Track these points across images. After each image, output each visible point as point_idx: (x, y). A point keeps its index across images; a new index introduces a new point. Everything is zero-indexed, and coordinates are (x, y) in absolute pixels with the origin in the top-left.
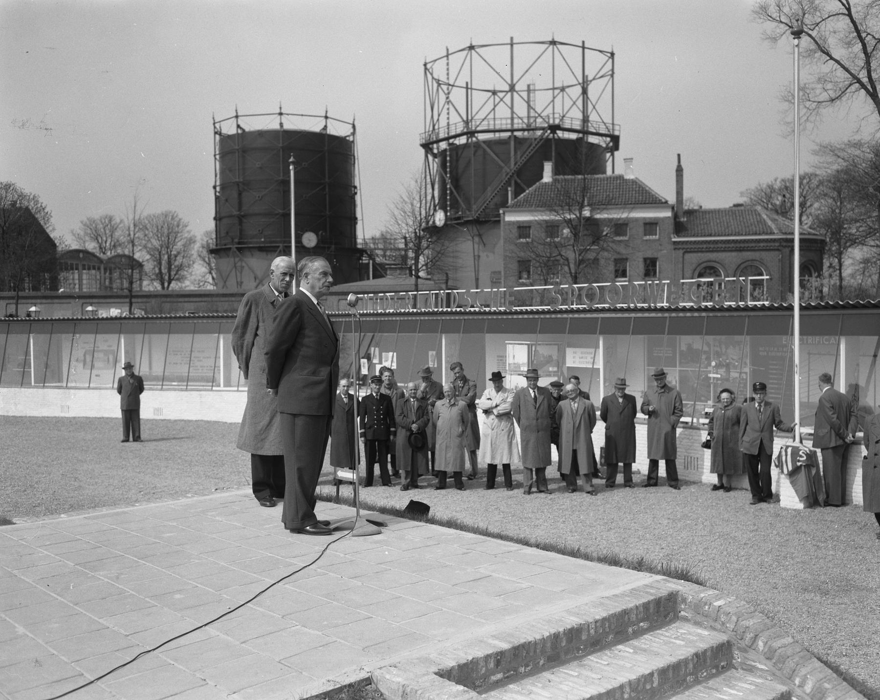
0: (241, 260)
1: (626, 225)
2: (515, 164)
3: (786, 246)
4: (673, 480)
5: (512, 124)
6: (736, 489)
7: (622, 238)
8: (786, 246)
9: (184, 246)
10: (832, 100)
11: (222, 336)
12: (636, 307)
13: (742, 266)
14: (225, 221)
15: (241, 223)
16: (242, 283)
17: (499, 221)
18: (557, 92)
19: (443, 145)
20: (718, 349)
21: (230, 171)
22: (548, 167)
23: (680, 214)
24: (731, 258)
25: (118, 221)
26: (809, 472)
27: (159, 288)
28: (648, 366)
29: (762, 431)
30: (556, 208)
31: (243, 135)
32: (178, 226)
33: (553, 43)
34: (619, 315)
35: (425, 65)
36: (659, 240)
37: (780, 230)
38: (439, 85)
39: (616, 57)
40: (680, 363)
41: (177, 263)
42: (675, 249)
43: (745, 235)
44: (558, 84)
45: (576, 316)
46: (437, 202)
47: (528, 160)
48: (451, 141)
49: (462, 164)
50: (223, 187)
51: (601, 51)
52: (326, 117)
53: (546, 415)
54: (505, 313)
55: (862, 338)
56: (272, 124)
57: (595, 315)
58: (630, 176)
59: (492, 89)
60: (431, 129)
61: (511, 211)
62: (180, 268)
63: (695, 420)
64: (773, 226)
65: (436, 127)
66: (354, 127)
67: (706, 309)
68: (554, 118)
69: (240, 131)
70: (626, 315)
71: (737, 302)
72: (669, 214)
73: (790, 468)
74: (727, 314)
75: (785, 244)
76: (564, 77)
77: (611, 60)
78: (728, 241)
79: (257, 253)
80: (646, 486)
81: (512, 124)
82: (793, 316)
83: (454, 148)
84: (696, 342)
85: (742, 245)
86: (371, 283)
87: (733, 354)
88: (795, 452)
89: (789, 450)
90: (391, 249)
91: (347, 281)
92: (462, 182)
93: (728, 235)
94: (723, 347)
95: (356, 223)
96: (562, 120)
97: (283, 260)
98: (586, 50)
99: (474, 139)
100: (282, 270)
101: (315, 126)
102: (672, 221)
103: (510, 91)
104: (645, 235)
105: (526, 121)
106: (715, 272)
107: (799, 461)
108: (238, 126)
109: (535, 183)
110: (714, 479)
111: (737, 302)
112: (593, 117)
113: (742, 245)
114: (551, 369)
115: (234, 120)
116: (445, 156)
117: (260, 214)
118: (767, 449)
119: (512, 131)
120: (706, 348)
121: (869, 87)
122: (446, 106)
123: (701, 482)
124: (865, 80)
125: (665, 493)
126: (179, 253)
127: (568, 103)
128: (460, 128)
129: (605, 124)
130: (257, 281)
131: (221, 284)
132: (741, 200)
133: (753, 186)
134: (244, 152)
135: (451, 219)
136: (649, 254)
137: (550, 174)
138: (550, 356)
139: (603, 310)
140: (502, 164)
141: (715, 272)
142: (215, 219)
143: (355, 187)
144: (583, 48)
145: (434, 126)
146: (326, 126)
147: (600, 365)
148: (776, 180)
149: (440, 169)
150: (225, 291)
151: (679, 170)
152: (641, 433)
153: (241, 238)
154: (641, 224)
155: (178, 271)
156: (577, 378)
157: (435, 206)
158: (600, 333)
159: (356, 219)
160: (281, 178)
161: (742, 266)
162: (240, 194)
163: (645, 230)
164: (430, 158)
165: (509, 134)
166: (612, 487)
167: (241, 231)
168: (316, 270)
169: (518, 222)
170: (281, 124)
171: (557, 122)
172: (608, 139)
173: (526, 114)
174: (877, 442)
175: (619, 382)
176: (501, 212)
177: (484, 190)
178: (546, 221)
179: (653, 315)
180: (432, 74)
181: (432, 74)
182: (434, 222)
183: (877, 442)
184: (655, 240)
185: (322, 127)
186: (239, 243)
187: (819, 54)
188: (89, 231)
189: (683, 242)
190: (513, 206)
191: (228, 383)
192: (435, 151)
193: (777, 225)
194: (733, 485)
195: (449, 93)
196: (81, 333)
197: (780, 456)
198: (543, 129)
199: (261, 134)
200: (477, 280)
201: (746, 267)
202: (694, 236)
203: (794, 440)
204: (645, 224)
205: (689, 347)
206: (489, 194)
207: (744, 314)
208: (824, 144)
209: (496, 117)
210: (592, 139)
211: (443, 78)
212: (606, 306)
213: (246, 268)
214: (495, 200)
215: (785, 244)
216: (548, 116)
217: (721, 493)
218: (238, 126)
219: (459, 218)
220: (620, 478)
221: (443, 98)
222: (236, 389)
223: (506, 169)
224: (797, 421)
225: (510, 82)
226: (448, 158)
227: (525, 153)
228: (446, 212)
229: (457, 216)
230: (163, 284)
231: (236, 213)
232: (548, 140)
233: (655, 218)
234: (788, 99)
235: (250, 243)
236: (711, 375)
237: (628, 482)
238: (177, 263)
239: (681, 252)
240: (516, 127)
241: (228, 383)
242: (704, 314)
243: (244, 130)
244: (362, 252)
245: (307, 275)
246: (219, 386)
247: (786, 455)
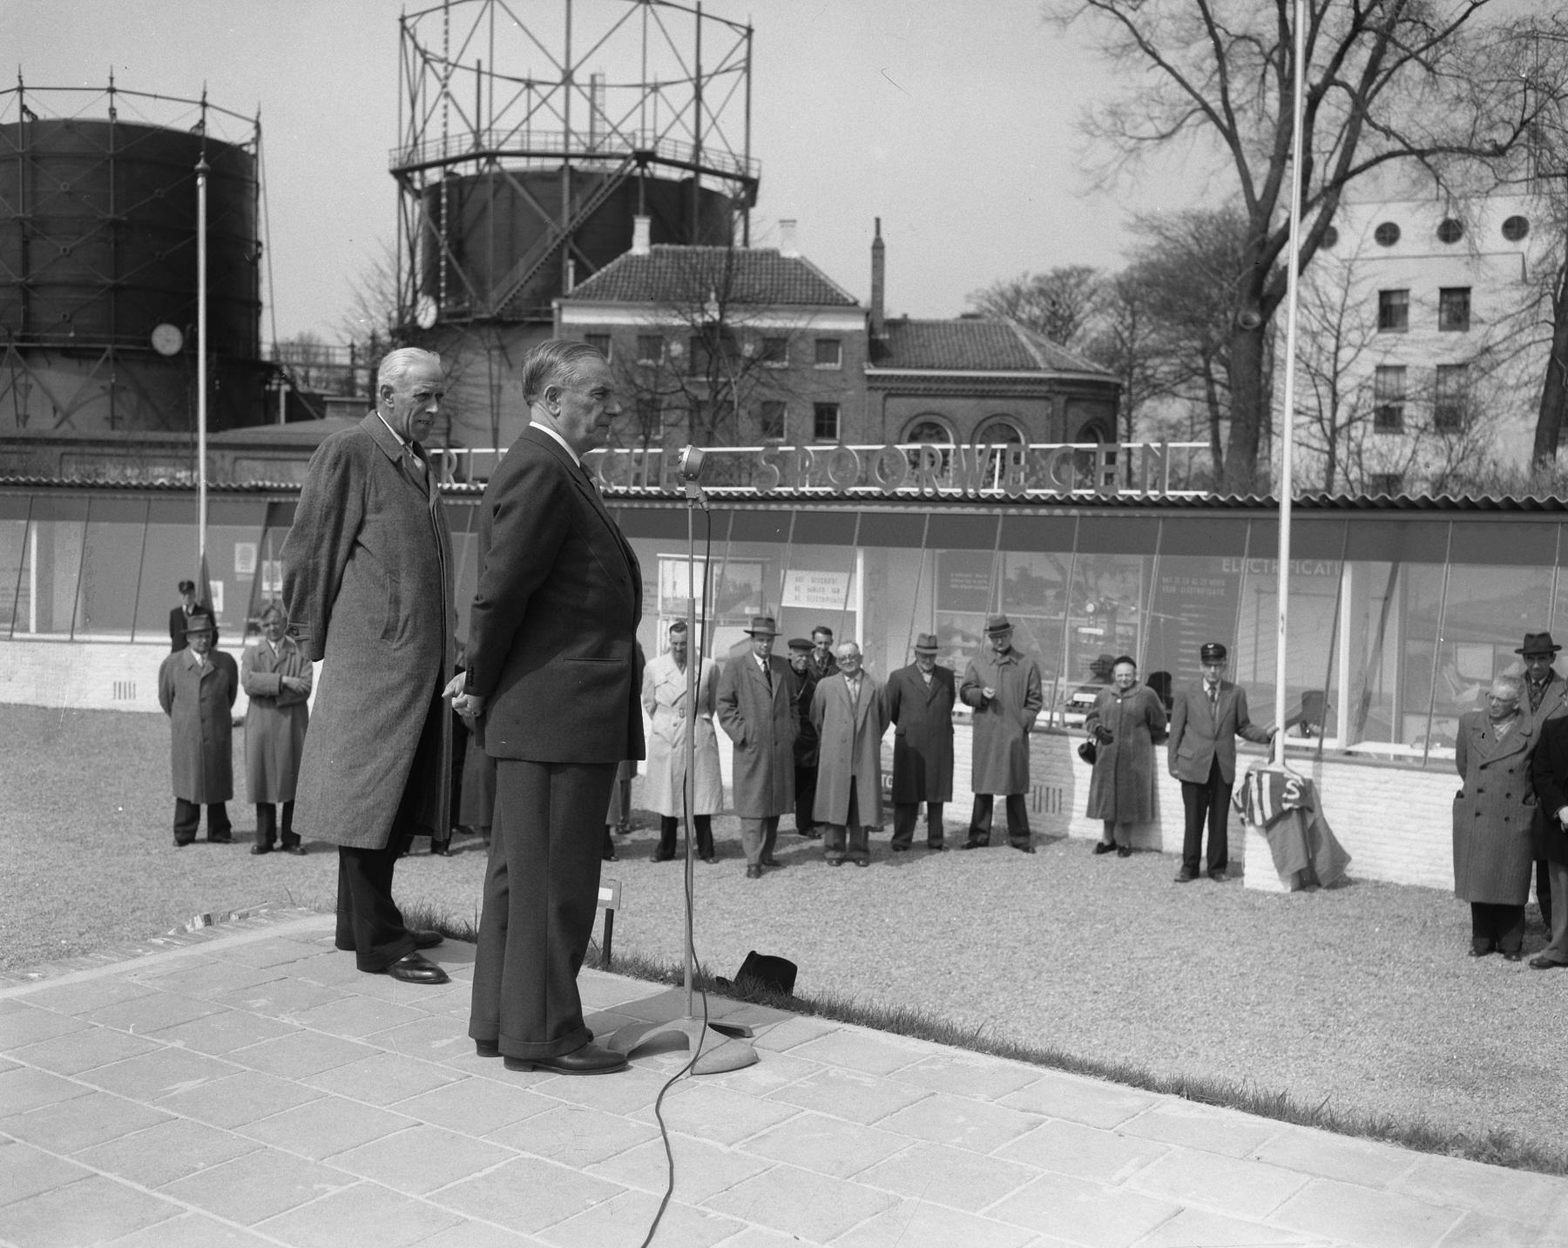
0: (25, 372)
2: (571, 219)
3: (1059, 393)
4: (1020, 834)
5: (567, 144)
6: (1139, 850)
8: (1059, 393)
10: (1163, 137)
11: (34, 526)
12: (936, 494)
13: (985, 425)
15: (27, 300)
16: (27, 417)
17: (550, 324)
18: (648, 90)
19: (434, 175)
20: (1081, 579)
22: (642, 227)
23: (878, 326)
24: (966, 410)
26: (1303, 822)
28: (941, 607)
29: (1216, 738)
30: (679, 304)
34: (900, 509)
35: (402, 20)
36: (841, 371)
37: (1050, 363)
38: (426, 61)
39: (755, 36)
40: (1004, 603)
42: (870, 389)
43: (992, 369)
44: (650, 80)
45: (810, 507)
46: (419, 281)
47: (595, 214)
48: (449, 167)
49: (471, 210)
51: (729, 24)
52: (204, 105)
53: (786, 702)
54: (659, 497)
55: (1374, 564)
57: (848, 508)
58: (790, 253)
59: (524, 76)
60: (411, 142)
61: (572, 305)
63: (1056, 717)
64: (1038, 357)
65: (420, 141)
66: (258, 126)
67: (1081, 502)
68: (644, 140)
69: (26, 119)
70: (914, 509)
71: (1144, 491)
72: (859, 324)
73: (1269, 815)
74: (1121, 513)
75: (1057, 388)
76: (664, 67)
77: (745, 42)
78: (963, 380)
80: (969, 847)
81: (567, 144)
82: (1277, 520)
83: (456, 183)
84: (1040, 565)
85: (986, 387)
86: (282, 430)
87: (1109, 587)
88: (1278, 782)
89: (1266, 779)
90: (319, 367)
91: (239, 423)
92: (470, 246)
93: (962, 368)
94: (1091, 575)
95: (259, 313)
96: (657, 140)
97: (412, 360)
98: (703, 19)
100: (416, 387)
102: (866, 338)
103: (562, 83)
104: (818, 361)
105: (587, 140)
106: (938, 433)
107: (1286, 801)
108: (24, 108)
109: (617, 256)
110: (1096, 830)
111: (1144, 491)
112: (711, 142)
113: (986, 387)
114: (747, 611)
115: (16, 95)
116: (439, 196)
118: (1224, 772)
119: (567, 156)
120: (1056, 577)
121: (1225, 122)
122: (442, 101)
123: (1066, 836)
124: (1216, 105)
125: (999, 861)
127: (665, 117)
128: (467, 145)
129: (734, 156)
130: (59, 415)
132: (971, 308)
133: (987, 284)
134: (34, 159)
135: (449, 316)
136: (825, 398)
138: (747, 586)
139: (868, 498)
140: (547, 219)
141: (938, 433)
143: (259, 244)
144: (699, 14)
145: (416, 139)
146: (202, 122)
147: (857, 605)
148: (1025, 276)
149: (427, 219)
151: (878, 248)
152: (963, 740)
153: (26, 329)
154: (812, 340)
156: (828, 632)
157: (415, 293)
158: (859, 544)
159: (259, 304)
160: (111, 216)
161: (985, 425)
162: (26, 243)
163: (817, 354)
164: (408, 198)
165: (559, 162)
166: (905, 849)
167: (27, 315)
168: (583, 382)
169: (587, 326)
170: (112, 111)
171: (649, 146)
172: (739, 185)
173: (587, 129)
174: (1483, 767)
175: (924, 643)
176: (555, 305)
177: (512, 263)
178: (641, 328)
179: (970, 510)
180: (413, 38)
181: (413, 38)
182: (414, 319)
183: (1483, 767)
184: (834, 372)
185: (195, 122)
186: (22, 339)
187: (1139, 53)
189: (885, 378)
190: (576, 296)
191: (45, 625)
192: (418, 185)
193: (1044, 354)
194: (1135, 840)
195: (447, 78)
196: (161, 520)
197: (1246, 789)
198: (624, 157)
199: (70, 126)
200: (496, 431)
201: (990, 427)
202: (903, 367)
203: (1272, 760)
204: (819, 341)
205: (1024, 574)
206: (522, 272)
207: (1154, 513)
208: (1143, 214)
209: (536, 130)
210: (707, 182)
211: (436, 49)
212: (875, 490)
213: (36, 391)
214: (532, 284)
215: (1057, 388)
216: (633, 134)
217: (1112, 857)
218: (24, 108)
219: (463, 314)
220: (921, 833)
221: (433, 87)
222: (67, 637)
223: (553, 227)
224: (1280, 721)
225: (563, 66)
226: (444, 200)
227: (589, 199)
228: (438, 300)
229: (460, 308)
232: (631, 179)
233: (837, 332)
234: (1088, 127)
235: (46, 340)
236: (1083, 630)
237: (937, 842)
239: (880, 395)
240: (573, 149)
241: (45, 625)
242: (1074, 512)
243: (34, 117)
244: (272, 369)
245: (554, 394)
246: (26, 629)
247: (1260, 789)
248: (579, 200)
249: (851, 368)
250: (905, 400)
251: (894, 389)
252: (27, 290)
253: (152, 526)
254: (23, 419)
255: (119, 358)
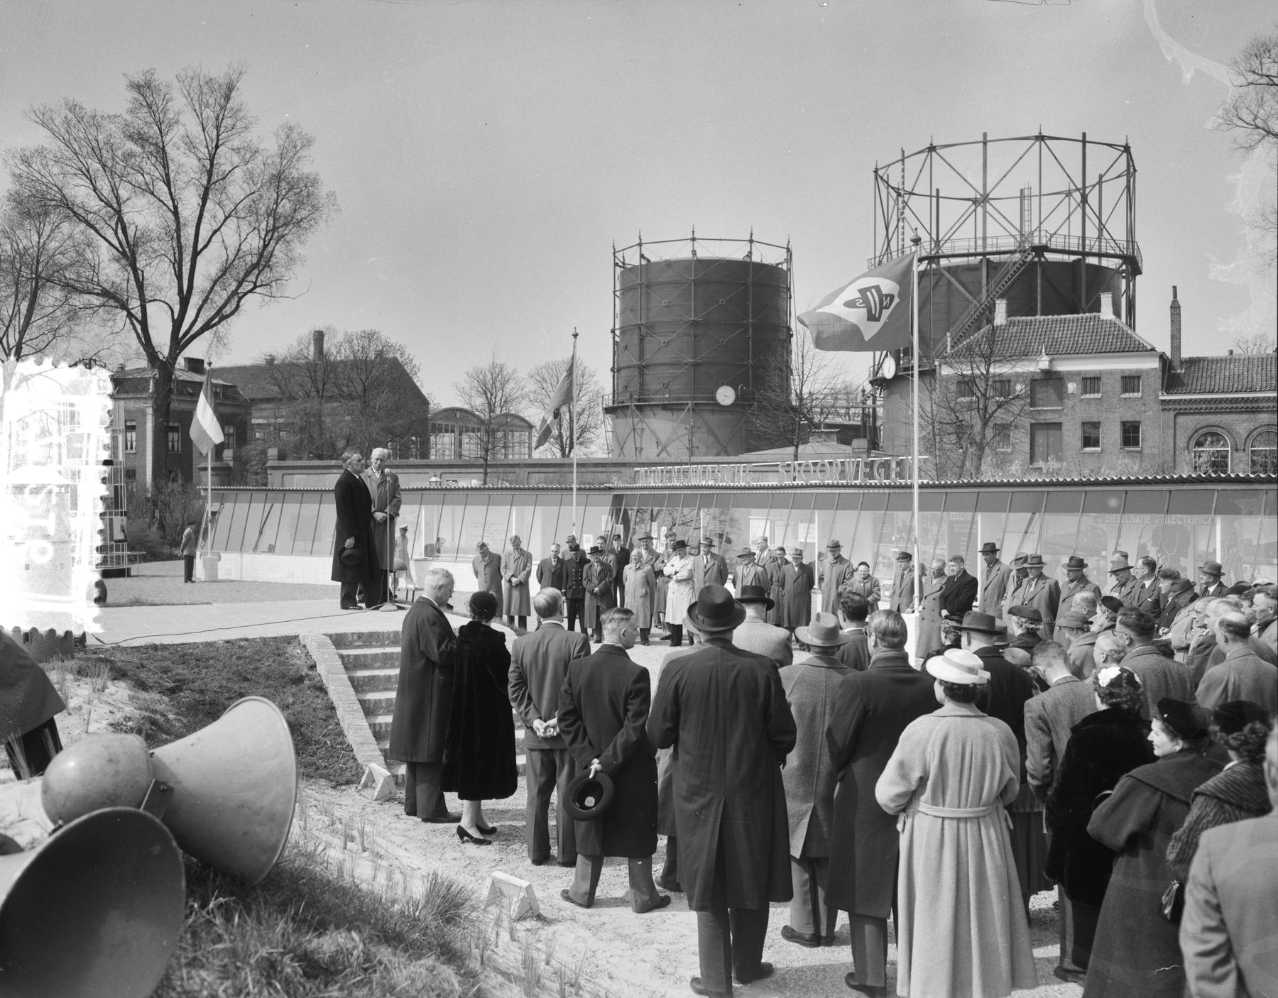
1: (1099, 379)
7: (1131, 395)
9: (590, 401)
13: (1255, 433)
14: (623, 373)
15: (642, 375)
21: (631, 310)
22: (1001, 306)
25: (510, 371)
27: (559, 455)
31: (648, 266)
32: (583, 376)
33: (1041, 138)
35: (876, 172)
38: (899, 195)
41: (581, 423)
50: (624, 331)
52: (751, 241)
56: (682, 252)
62: (583, 430)
66: (788, 250)
69: (644, 262)
72: (1155, 364)
78: (1206, 401)
79: (660, 413)
99: (934, 266)
101: (736, 253)
108: (642, 256)
115: (637, 248)
117: (664, 364)
119: (984, 254)
126: (583, 410)
131: (617, 451)
136: (1129, 417)
137: (1004, 315)
142: (612, 370)
144: (1084, 142)
146: (750, 253)
150: (620, 460)
151: (1175, 308)
154: (1118, 377)
155: (583, 432)
161: (1255, 433)
162: (642, 339)
167: (642, 384)
170: (694, 252)
171: (1044, 241)
176: (937, 363)
186: (639, 400)
188: (476, 384)
189: (1175, 401)
199: (669, 264)
204: (1124, 378)
213: (647, 431)
218: (642, 256)
230: (563, 450)
231: (636, 362)
232: (1032, 264)
238: (581, 423)
240: (989, 250)
243: (649, 261)
248: (992, 283)
249: (1152, 391)
250: (1191, 417)
251: (1182, 410)
252: (642, 369)
253: (1126, 516)
254: (639, 450)
255: (696, 409)
